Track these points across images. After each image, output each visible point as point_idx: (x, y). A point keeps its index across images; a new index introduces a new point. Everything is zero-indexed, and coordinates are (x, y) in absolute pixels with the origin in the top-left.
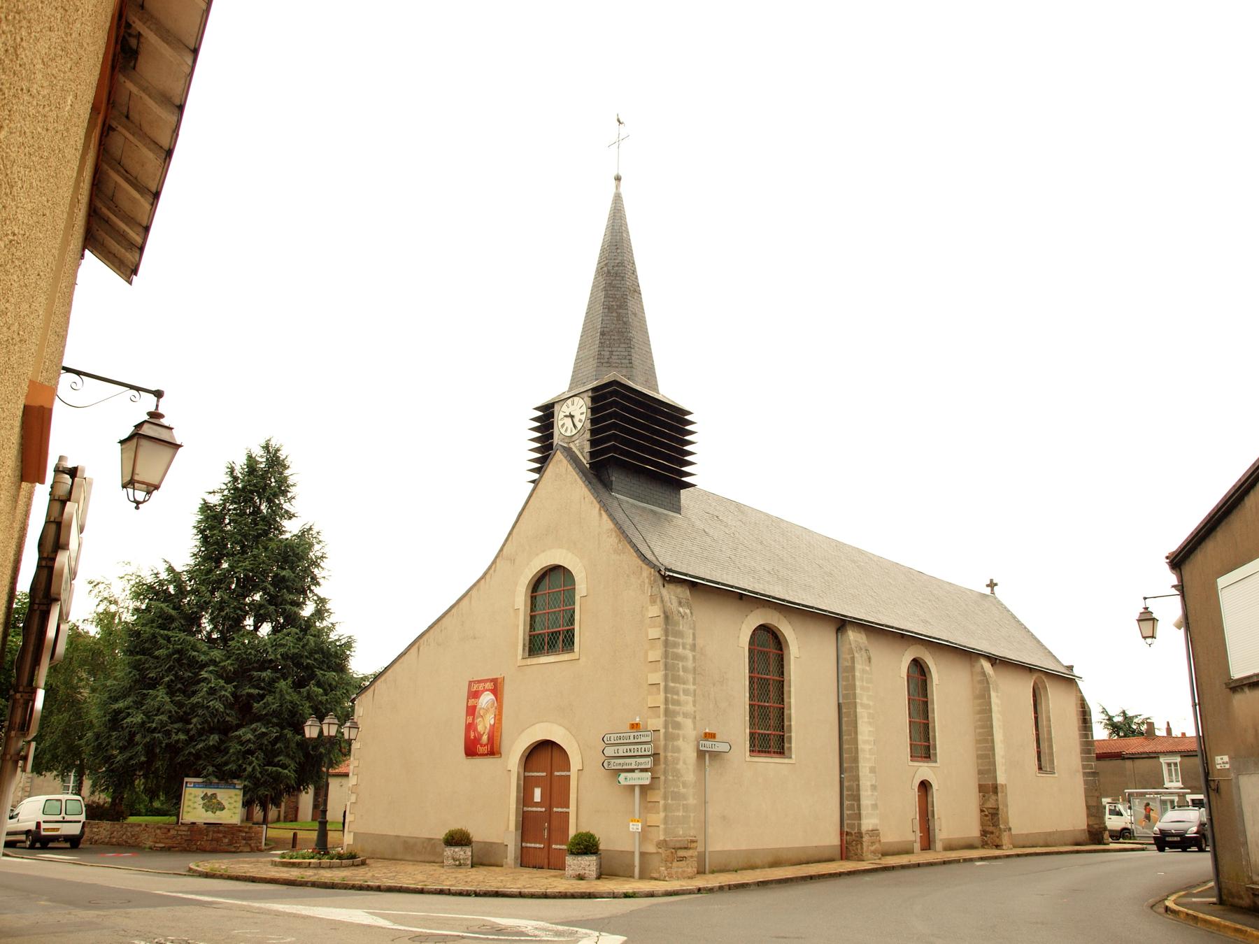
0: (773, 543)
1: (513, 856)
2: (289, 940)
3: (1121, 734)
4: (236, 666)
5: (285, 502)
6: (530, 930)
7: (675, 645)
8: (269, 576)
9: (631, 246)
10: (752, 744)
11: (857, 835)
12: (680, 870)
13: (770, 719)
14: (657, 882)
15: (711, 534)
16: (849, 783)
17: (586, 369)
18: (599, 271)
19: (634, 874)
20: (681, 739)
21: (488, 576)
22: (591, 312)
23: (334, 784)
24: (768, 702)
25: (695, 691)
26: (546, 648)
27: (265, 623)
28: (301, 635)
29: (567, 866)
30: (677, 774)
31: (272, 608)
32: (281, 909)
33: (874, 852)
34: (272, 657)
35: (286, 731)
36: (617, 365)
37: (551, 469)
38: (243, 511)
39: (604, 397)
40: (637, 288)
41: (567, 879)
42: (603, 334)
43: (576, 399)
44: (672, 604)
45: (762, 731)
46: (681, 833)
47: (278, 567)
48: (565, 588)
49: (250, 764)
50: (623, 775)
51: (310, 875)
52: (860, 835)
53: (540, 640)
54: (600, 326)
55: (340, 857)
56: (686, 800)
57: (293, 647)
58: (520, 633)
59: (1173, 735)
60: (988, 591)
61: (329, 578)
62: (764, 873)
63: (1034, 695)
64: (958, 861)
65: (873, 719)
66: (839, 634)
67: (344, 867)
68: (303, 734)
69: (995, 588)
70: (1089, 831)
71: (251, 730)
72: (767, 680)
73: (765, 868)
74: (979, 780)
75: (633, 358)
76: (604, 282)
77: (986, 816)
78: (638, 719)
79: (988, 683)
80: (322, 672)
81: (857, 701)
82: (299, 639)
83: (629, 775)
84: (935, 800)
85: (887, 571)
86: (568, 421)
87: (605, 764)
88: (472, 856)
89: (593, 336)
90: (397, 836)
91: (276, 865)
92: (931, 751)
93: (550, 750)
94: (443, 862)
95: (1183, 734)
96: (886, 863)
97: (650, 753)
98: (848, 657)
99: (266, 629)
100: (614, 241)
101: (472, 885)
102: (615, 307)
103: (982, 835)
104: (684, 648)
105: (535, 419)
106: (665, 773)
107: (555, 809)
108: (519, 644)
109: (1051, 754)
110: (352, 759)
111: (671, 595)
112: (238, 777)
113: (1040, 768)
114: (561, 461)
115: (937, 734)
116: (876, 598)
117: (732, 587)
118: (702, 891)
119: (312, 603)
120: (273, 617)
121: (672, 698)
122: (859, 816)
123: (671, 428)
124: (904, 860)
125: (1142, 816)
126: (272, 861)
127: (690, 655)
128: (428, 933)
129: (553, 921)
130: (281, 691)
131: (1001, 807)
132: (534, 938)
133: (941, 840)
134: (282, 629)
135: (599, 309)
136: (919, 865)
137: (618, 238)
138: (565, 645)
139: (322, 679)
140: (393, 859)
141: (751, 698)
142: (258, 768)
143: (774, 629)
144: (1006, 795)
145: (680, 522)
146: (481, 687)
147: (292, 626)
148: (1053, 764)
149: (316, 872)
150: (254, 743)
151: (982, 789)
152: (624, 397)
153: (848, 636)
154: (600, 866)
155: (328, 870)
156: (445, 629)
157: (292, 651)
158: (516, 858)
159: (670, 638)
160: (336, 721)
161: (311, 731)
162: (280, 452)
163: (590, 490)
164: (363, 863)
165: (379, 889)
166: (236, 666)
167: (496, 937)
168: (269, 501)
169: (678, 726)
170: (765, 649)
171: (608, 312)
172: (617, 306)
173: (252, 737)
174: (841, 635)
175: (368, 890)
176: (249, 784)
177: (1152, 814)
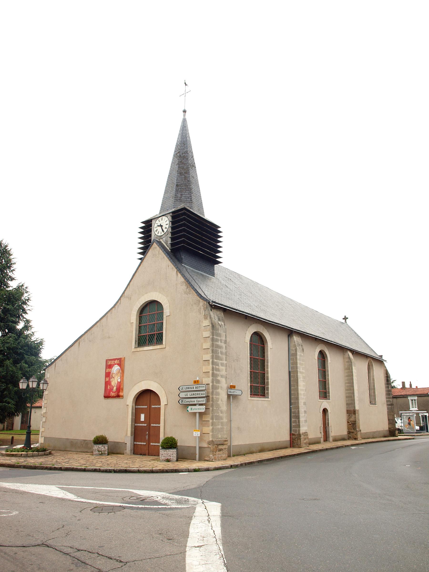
1: (130, 449)
6: (159, 499)
7: (217, 340)
10: (251, 391)
11: (298, 435)
13: (258, 379)
14: (208, 462)
17: (168, 203)
18: (175, 156)
19: (196, 459)
20: (220, 388)
21: (116, 306)
22: (171, 175)
25: (226, 364)
26: (147, 342)
28: (17, 337)
30: (218, 406)
32: (7, 487)
33: (306, 443)
34: (2, 349)
36: (184, 201)
37: (150, 253)
39: (179, 216)
41: (161, 461)
42: (177, 186)
43: (164, 217)
44: (215, 320)
45: (255, 385)
46: (220, 436)
48: (157, 312)
50: (190, 407)
51: (22, 461)
52: (299, 435)
53: (144, 339)
55: (37, 450)
56: (222, 420)
59: (412, 387)
61: (31, 310)
64: (342, 447)
65: (305, 379)
69: (347, 320)
70: (389, 431)
73: (257, 453)
76: (178, 161)
77: (350, 424)
78: (198, 378)
79: (351, 363)
80: (28, 356)
81: (298, 370)
82: (16, 340)
83: (193, 407)
84: (329, 417)
86: (159, 229)
87: (180, 402)
88: (108, 449)
91: (3, 456)
92: (327, 395)
93: (149, 394)
94: (93, 452)
95: (417, 387)
97: (205, 396)
98: (294, 349)
100: (183, 141)
102: (184, 173)
103: (348, 434)
104: (221, 342)
106: (212, 406)
107: (152, 425)
110: (43, 399)
111: (215, 315)
114: (156, 248)
115: (330, 386)
118: (233, 467)
120: (3, 329)
121: (215, 367)
122: (299, 426)
123: (211, 233)
125: (407, 423)
127: (224, 345)
128: (101, 504)
129: (172, 491)
130: (7, 365)
131: (357, 420)
133: (332, 436)
134: (6, 335)
135: (175, 174)
136: (332, 449)
137: (185, 140)
138: (150, 342)
139: (28, 360)
144: (359, 415)
145: (215, 281)
146: (112, 362)
151: (348, 412)
152: (189, 216)
154: (177, 454)
155: (31, 458)
156: (93, 333)
158: (131, 450)
159: (215, 337)
160: (36, 380)
161: (23, 385)
162: (8, 247)
163: (171, 262)
164: (50, 453)
165: (61, 469)
169: (218, 382)
171: (180, 175)
172: (184, 172)
177: (411, 422)
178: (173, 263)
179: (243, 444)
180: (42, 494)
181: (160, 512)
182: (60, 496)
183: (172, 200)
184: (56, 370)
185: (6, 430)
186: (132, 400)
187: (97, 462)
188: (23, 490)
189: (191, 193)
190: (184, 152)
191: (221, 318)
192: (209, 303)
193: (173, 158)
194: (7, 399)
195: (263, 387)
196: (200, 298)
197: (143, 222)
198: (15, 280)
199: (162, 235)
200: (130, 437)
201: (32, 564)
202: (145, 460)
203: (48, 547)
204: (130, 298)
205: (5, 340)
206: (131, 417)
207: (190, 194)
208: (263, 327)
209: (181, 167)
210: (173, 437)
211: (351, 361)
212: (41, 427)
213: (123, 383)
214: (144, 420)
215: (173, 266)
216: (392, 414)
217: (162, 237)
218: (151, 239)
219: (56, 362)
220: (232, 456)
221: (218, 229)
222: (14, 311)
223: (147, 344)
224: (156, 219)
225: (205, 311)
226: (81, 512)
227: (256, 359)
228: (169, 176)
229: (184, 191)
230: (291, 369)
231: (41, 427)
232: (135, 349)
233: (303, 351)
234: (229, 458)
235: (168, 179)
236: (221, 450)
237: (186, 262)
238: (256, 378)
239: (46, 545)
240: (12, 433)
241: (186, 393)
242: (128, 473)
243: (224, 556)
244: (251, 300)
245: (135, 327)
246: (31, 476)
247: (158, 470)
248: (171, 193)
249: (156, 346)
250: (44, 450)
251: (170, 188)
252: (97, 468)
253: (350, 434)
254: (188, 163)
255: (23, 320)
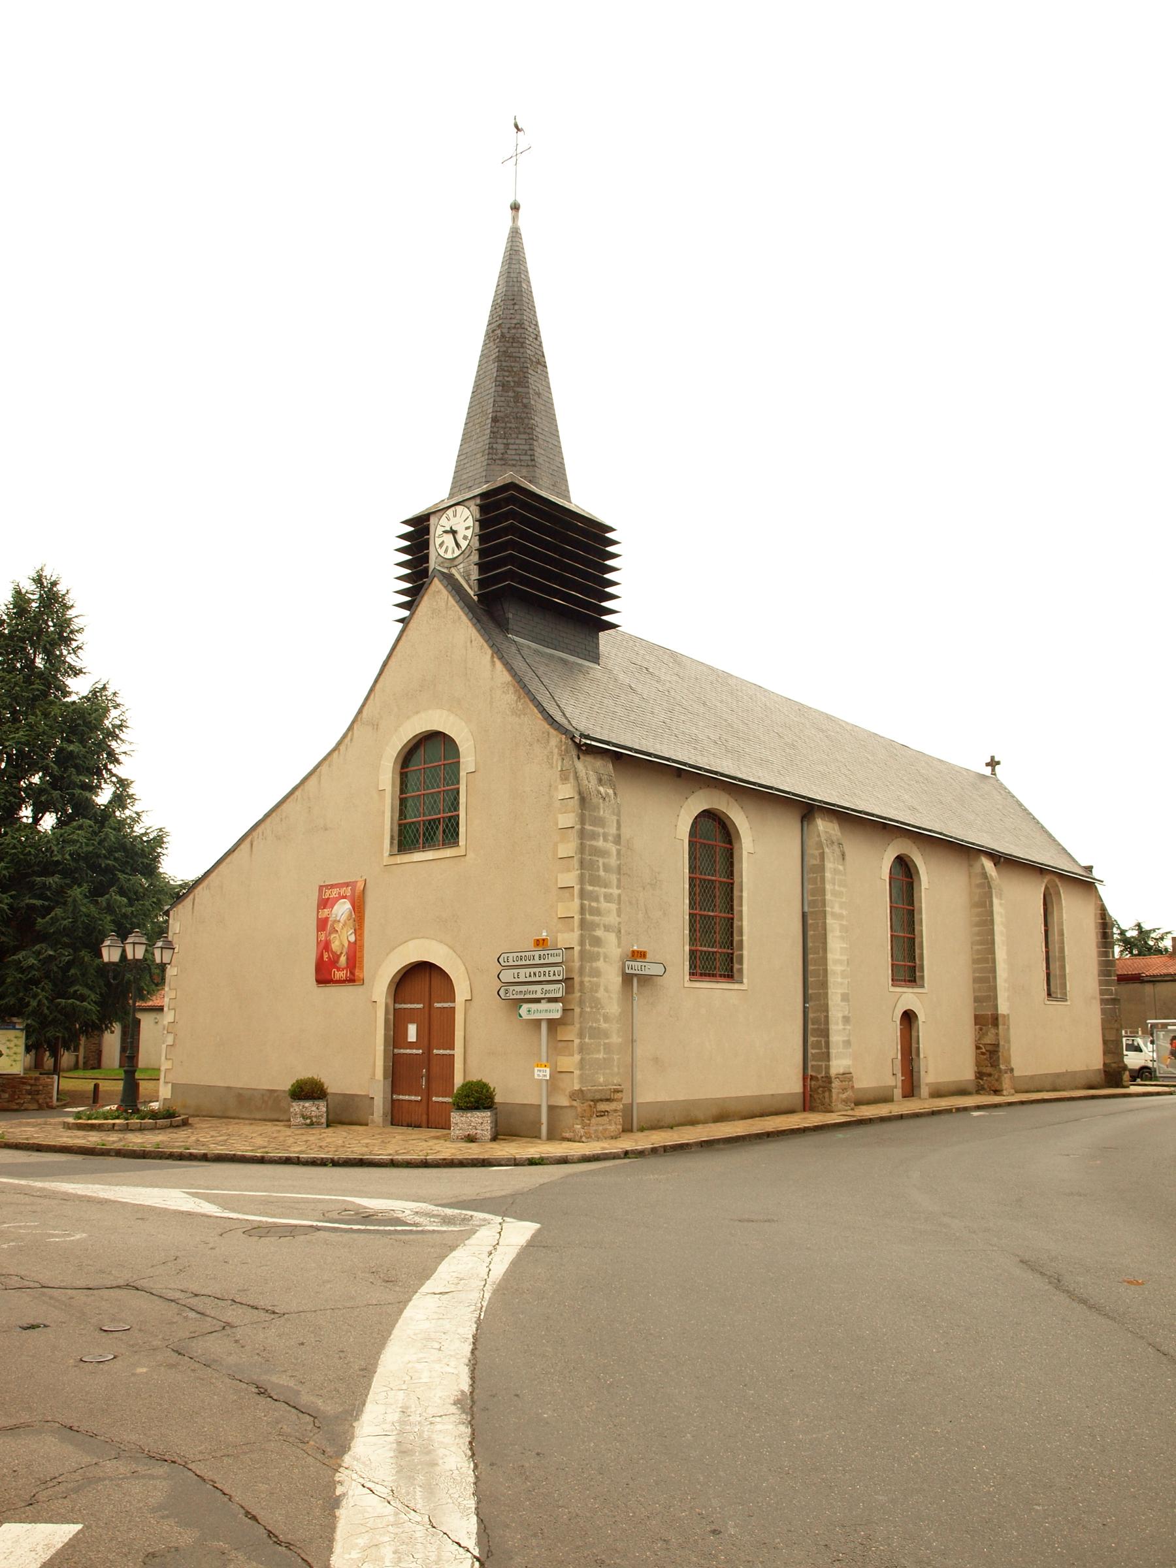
0: (719, 704)
1: (382, 1112)
2: (78, 1237)
3: (1135, 952)
4: (12, 871)
5: (69, 653)
7: (594, 836)
8: (51, 752)
9: (533, 302)
11: (824, 1079)
12: (601, 1128)
13: (715, 933)
14: (571, 1143)
15: (639, 691)
16: (815, 1015)
17: (472, 468)
18: (490, 335)
21: (342, 748)
22: (479, 391)
23: (147, 1022)
24: (713, 911)
25: (619, 896)
27: (48, 813)
28: (96, 829)
29: (452, 1125)
30: (597, 1004)
31: (56, 794)
32: (71, 1191)
33: (845, 1101)
34: (59, 858)
35: (83, 953)
36: (514, 462)
37: (426, 604)
38: (11, 666)
39: (497, 505)
40: (541, 359)
41: (453, 1141)
42: (495, 420)
43: (460, 508)
45: (705, 949)
46: (601, 1080)
47: (62, 739)
48: (446, 762)
49: (35, 996)
50: (525, 1007)
51: (113, 1140)
52: (828, 1079)
53: (413, 831)
54: (491, 410)
55: (154, 1115)
56: (608, 1038)
57: (87, 845)
58: (386, 822)
60: (987, 771)
61: (131, 753)
62: (708, 1129)
63: (1045, 904)
64: (948, 1111)
66: (805, 823)
67: (159, 1129)
68: (101, 956)
70: (1105, 1071)
71: (34, 953)
72: (712, 881)
74: (975, 1009)
75: (536, 454)
76: (497, 350)
77: (983, 1054)
79: (990, 887)
80: (125, 876)
81: (827, 909)
82: (95, 833)
83: (534, 1006)
84: (920, 1034)
85: (862, 743)
88: (327, 1111)
89: (483, 424)
90: (228, 1087)
92: (918, 974)
93: (427, 975)
96: (861, 1114)
97: (560, 978)
98: (817, 853)
99: (48, 821)
100: (510, 293)
101: (328, 1152)
102: (512, 384)
103: (977, 1078)
104: (605, 840)
105: (403, 537)
106: (581, 1002)
107: (435, 1051)
108: (385, 836)
109: (1063, 976)
110: (167, 989)
111: (587, 769)
112: (19, 1014)
113: (1049, 995)
115: (925, 952)
116: (851, 777)
117: (668, 759)
119: (109, 786)
120: (59, 806)
121: (590, 905)
122: (827, 1057)
123: (588, 549)
124: (883, 1110)
126: (64, 1122)
127: (613, 849)
128: (270, 1223)
130: (75, 901)
131: (1002, 1043)
132: (414, 1228)
133: (927, 1084)
135: (490, 386)
136: (901, 1117)
137: (516, 289)
138: (427, 839)
139: (126, 885)
140: (224, 1116)
141: (692, 905)
142: (46, 1002)
143: (722, 817)
144: (1008, 1028)
145: (598, 675)
146: (334, 893)
147: (85, 817)
148: (1066, 989)
149: (121, 1136)
150: (38, 970)
151: (979, 1020)
152: (525, 506)
153: (817, 826)
154: (496, 1123)
155: (138, 1134)
156: (285, 818)
157: (85, 850)
159: (588, 827)
160: (144, 940)
161: (110, 954)
163: (478, 631)
164: (185, 1123)
165: (205, 1158)
166: (12, 871)
167: (363, 1227)
168: (49, 654)
169: (597, 942)
170: (710, 842)
171: (503, 390)
172: (514, 382)
173: (35, 962)
174: (808, 825)
175: (191, 1160)
176: (34, 1023)
178: (483, 632)
179: (667, 1099)
180: (146, 1204)
181: (393, 1237)
182: (184, 1208)
183: (482, 462)
184: (195, 912)
185: (84, 1070)
186: (385, 989)
187: (296, 1143)
188: (106, 1197)
189: (531, 439)
190: (513, 325)
191: (605, 777)
192: (573, 738)
193: (485, 341)
194: (76, 988)
195: (728, 954)
196: (551, 725)
197: (407, 522)
198: (85, 673)
199: (457, 557)
200: (382, 1083)
201: (100, 1314)
202: (416, 1137)
203: (137, 1289)
204: (376, 726)
205: (66, 835)
206: (383, 1032)
207: (531, 441)
208: (727, 796)
209: (506, 368)
210: (483, 1080)
211: (989, 882)
212: (163, 1058)
213: (362, 946)
214: (415, 1040)
215: (482, 641)
216: (1116, 1026)
217: (456, 563)
218: (428, 567)
219: (196, 891)
220: (638, 1130)
221: (608, 535)
222: (85, 758)
223: (421, 845)
224: (441, 513)
225: (563, 759)
226: (221, 1235)
227: (709, 880)
228: (475, 394)
229: (514, 436)
230: (809, 907)
231: (163, 1058)
232: (392, 857)
233: (843, 859)
234: (625, 1136)
235: (471, 403)
236: (605, 1115)
237: (521, 630)
238: (707, 932)
239: (133, 1287)
240: (97, 1076)
241: (516, 971)
242: (368, 1166)
243: (484, 1309)
244: (701, 724)
245: (390, 801)
246: (128, 1171)
247: (440, 1159)
248: (480, 439)
249: (441, 850)
250: (170, 1114)
251: (477, 426)
252: (291, 1155)
253: (982, 1080)
254: (524, 355)
255: (111, 781)
